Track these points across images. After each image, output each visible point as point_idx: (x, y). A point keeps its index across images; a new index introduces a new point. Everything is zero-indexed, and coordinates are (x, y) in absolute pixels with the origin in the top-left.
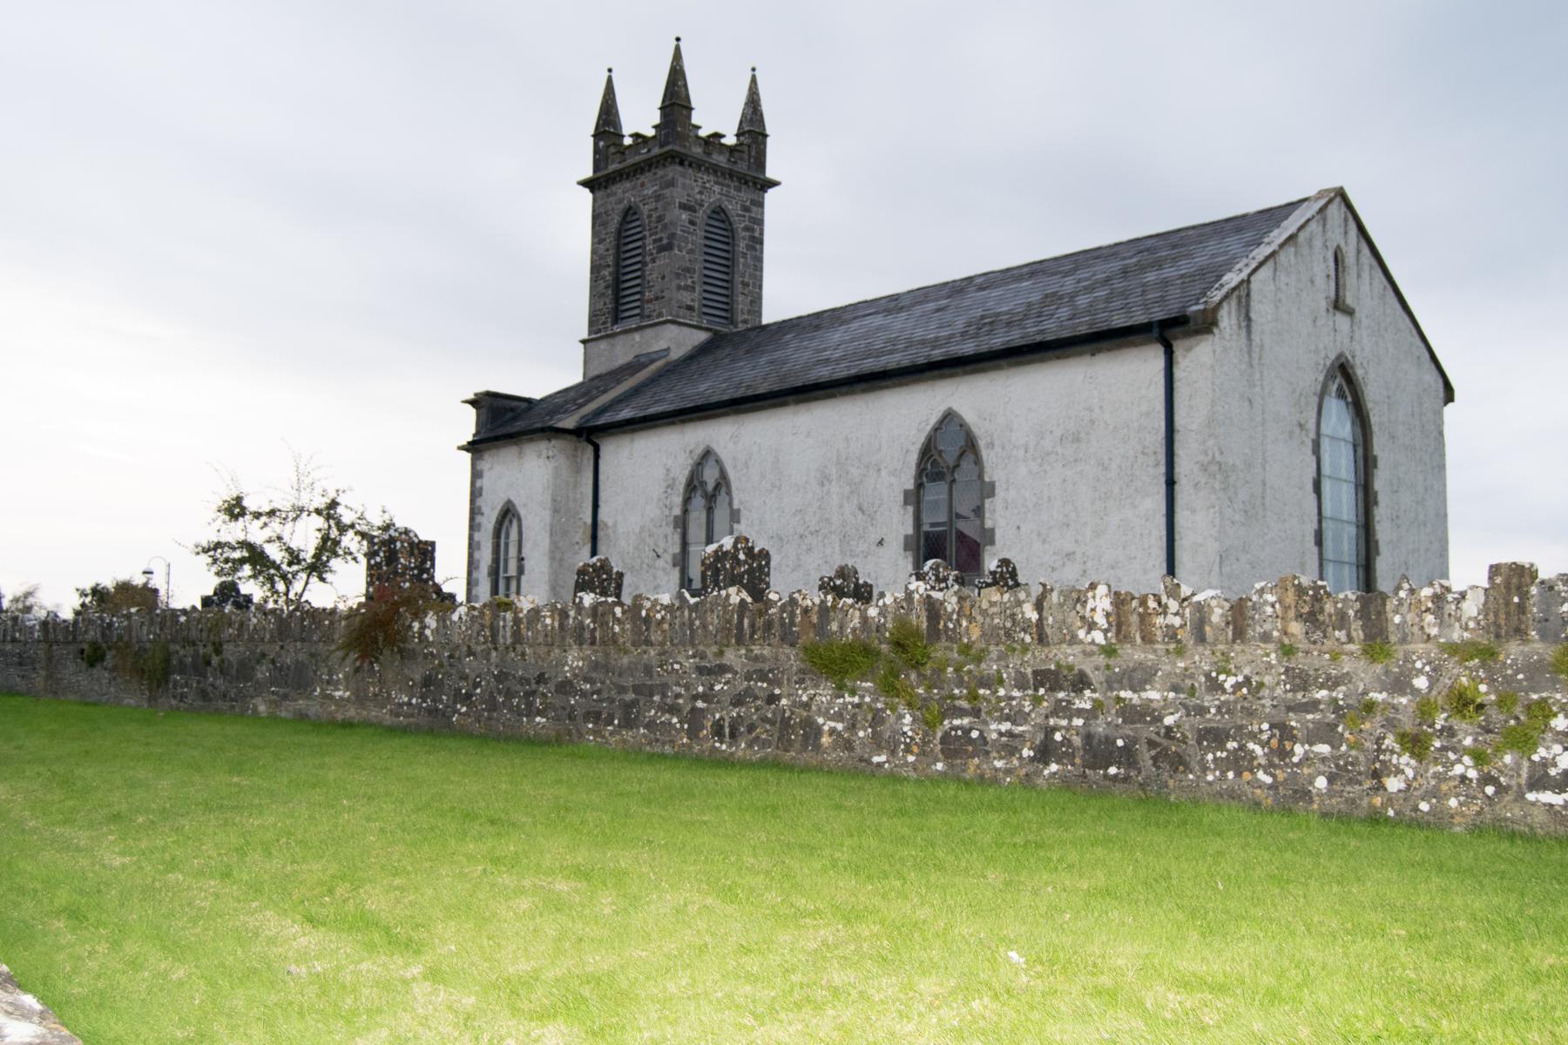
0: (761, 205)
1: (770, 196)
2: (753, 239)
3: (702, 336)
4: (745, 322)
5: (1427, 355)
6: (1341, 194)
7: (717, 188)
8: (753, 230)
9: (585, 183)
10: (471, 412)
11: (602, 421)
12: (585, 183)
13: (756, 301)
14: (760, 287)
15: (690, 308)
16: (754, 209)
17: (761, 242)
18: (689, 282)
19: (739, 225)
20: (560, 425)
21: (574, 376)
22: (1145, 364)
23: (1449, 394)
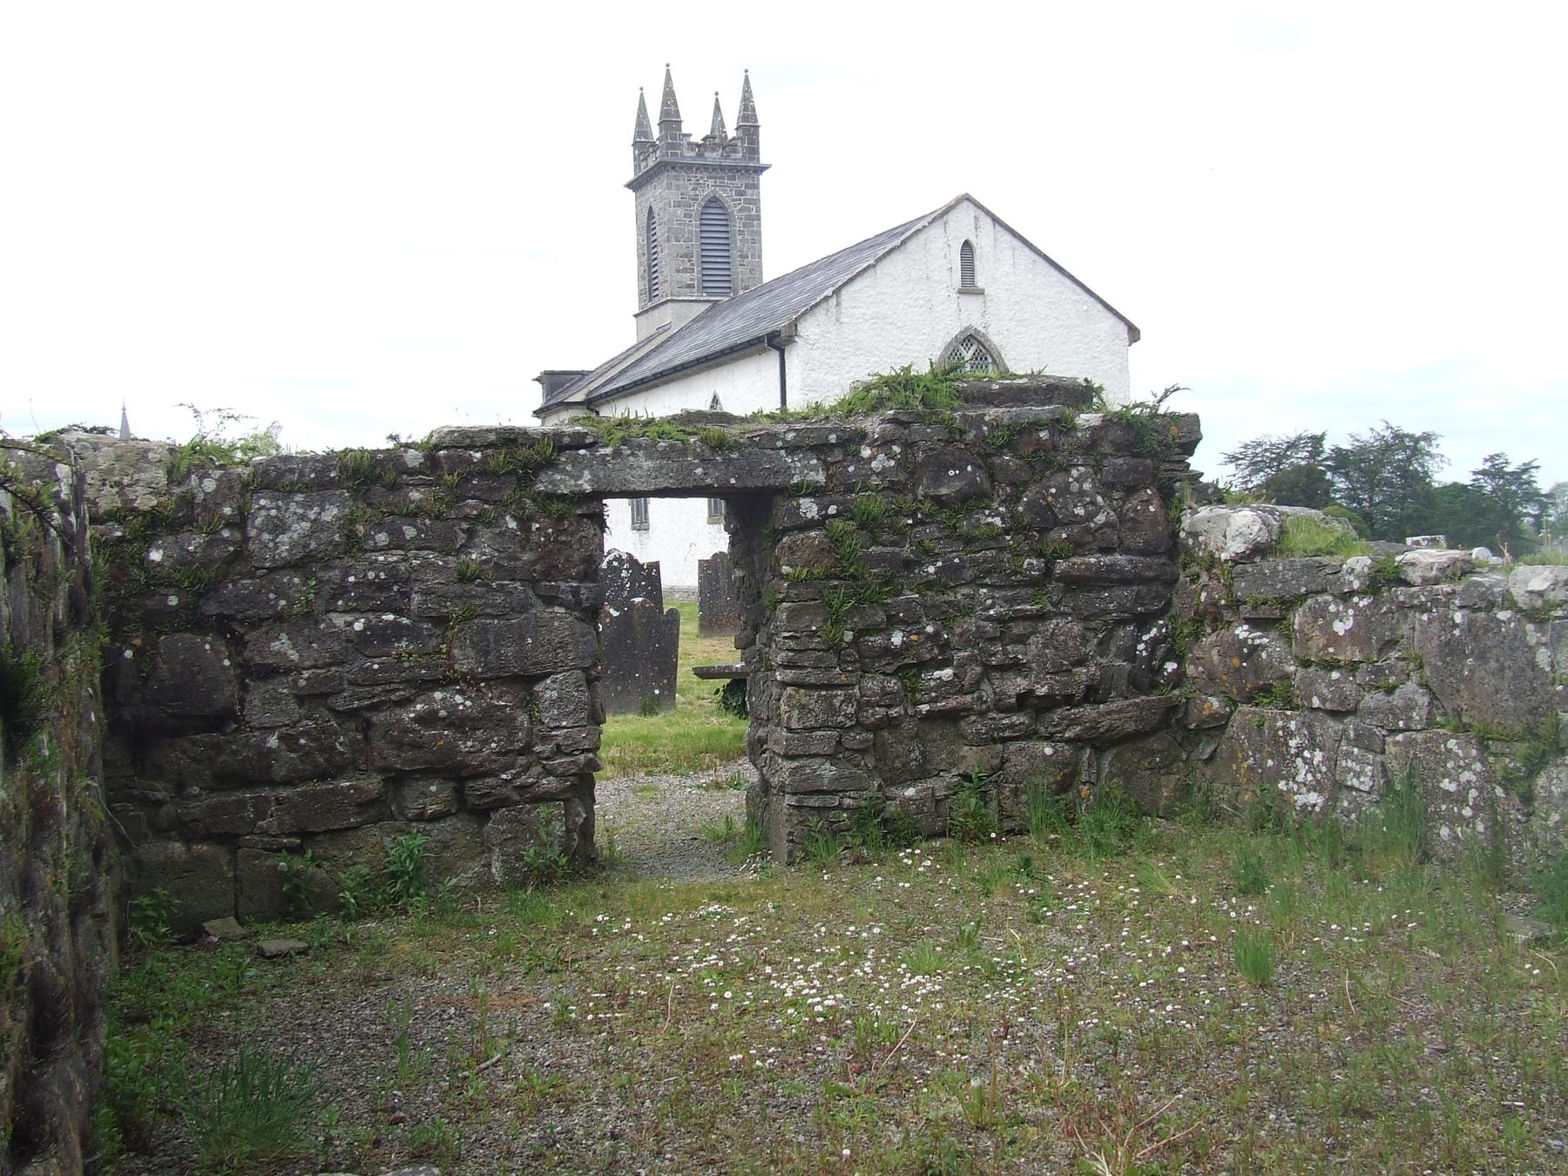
0: (756, 187)
1: (764, 178)
2: (750, 218)
3: (706, 306)
4: (746, 288)
5: (1100, 307)
6: (968, 198)
7: (711, 182)
8: (749, 210)
9: (629, 186)
10: (538, 387)
11: (604, 391)
12: (629, 186)
13: (757, 269)
14: (760, 256)
15: (689, 286)
16: (749, 191)
17: (758, 218)
18: (688, 265)
19: (734, 209)
20: (571, 400)
21: (633, 342)
22: (771, 362)
23: (1134, 334)
